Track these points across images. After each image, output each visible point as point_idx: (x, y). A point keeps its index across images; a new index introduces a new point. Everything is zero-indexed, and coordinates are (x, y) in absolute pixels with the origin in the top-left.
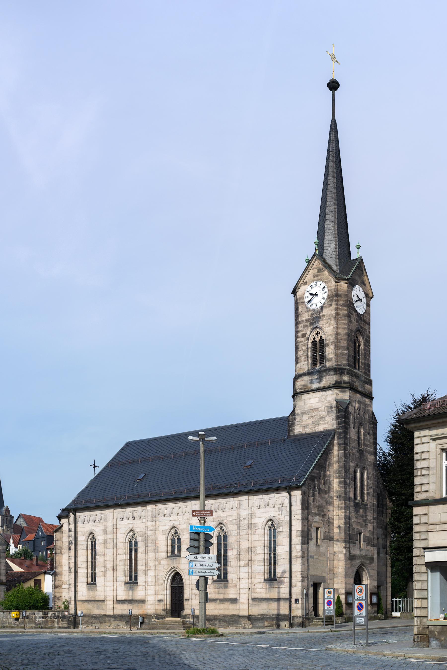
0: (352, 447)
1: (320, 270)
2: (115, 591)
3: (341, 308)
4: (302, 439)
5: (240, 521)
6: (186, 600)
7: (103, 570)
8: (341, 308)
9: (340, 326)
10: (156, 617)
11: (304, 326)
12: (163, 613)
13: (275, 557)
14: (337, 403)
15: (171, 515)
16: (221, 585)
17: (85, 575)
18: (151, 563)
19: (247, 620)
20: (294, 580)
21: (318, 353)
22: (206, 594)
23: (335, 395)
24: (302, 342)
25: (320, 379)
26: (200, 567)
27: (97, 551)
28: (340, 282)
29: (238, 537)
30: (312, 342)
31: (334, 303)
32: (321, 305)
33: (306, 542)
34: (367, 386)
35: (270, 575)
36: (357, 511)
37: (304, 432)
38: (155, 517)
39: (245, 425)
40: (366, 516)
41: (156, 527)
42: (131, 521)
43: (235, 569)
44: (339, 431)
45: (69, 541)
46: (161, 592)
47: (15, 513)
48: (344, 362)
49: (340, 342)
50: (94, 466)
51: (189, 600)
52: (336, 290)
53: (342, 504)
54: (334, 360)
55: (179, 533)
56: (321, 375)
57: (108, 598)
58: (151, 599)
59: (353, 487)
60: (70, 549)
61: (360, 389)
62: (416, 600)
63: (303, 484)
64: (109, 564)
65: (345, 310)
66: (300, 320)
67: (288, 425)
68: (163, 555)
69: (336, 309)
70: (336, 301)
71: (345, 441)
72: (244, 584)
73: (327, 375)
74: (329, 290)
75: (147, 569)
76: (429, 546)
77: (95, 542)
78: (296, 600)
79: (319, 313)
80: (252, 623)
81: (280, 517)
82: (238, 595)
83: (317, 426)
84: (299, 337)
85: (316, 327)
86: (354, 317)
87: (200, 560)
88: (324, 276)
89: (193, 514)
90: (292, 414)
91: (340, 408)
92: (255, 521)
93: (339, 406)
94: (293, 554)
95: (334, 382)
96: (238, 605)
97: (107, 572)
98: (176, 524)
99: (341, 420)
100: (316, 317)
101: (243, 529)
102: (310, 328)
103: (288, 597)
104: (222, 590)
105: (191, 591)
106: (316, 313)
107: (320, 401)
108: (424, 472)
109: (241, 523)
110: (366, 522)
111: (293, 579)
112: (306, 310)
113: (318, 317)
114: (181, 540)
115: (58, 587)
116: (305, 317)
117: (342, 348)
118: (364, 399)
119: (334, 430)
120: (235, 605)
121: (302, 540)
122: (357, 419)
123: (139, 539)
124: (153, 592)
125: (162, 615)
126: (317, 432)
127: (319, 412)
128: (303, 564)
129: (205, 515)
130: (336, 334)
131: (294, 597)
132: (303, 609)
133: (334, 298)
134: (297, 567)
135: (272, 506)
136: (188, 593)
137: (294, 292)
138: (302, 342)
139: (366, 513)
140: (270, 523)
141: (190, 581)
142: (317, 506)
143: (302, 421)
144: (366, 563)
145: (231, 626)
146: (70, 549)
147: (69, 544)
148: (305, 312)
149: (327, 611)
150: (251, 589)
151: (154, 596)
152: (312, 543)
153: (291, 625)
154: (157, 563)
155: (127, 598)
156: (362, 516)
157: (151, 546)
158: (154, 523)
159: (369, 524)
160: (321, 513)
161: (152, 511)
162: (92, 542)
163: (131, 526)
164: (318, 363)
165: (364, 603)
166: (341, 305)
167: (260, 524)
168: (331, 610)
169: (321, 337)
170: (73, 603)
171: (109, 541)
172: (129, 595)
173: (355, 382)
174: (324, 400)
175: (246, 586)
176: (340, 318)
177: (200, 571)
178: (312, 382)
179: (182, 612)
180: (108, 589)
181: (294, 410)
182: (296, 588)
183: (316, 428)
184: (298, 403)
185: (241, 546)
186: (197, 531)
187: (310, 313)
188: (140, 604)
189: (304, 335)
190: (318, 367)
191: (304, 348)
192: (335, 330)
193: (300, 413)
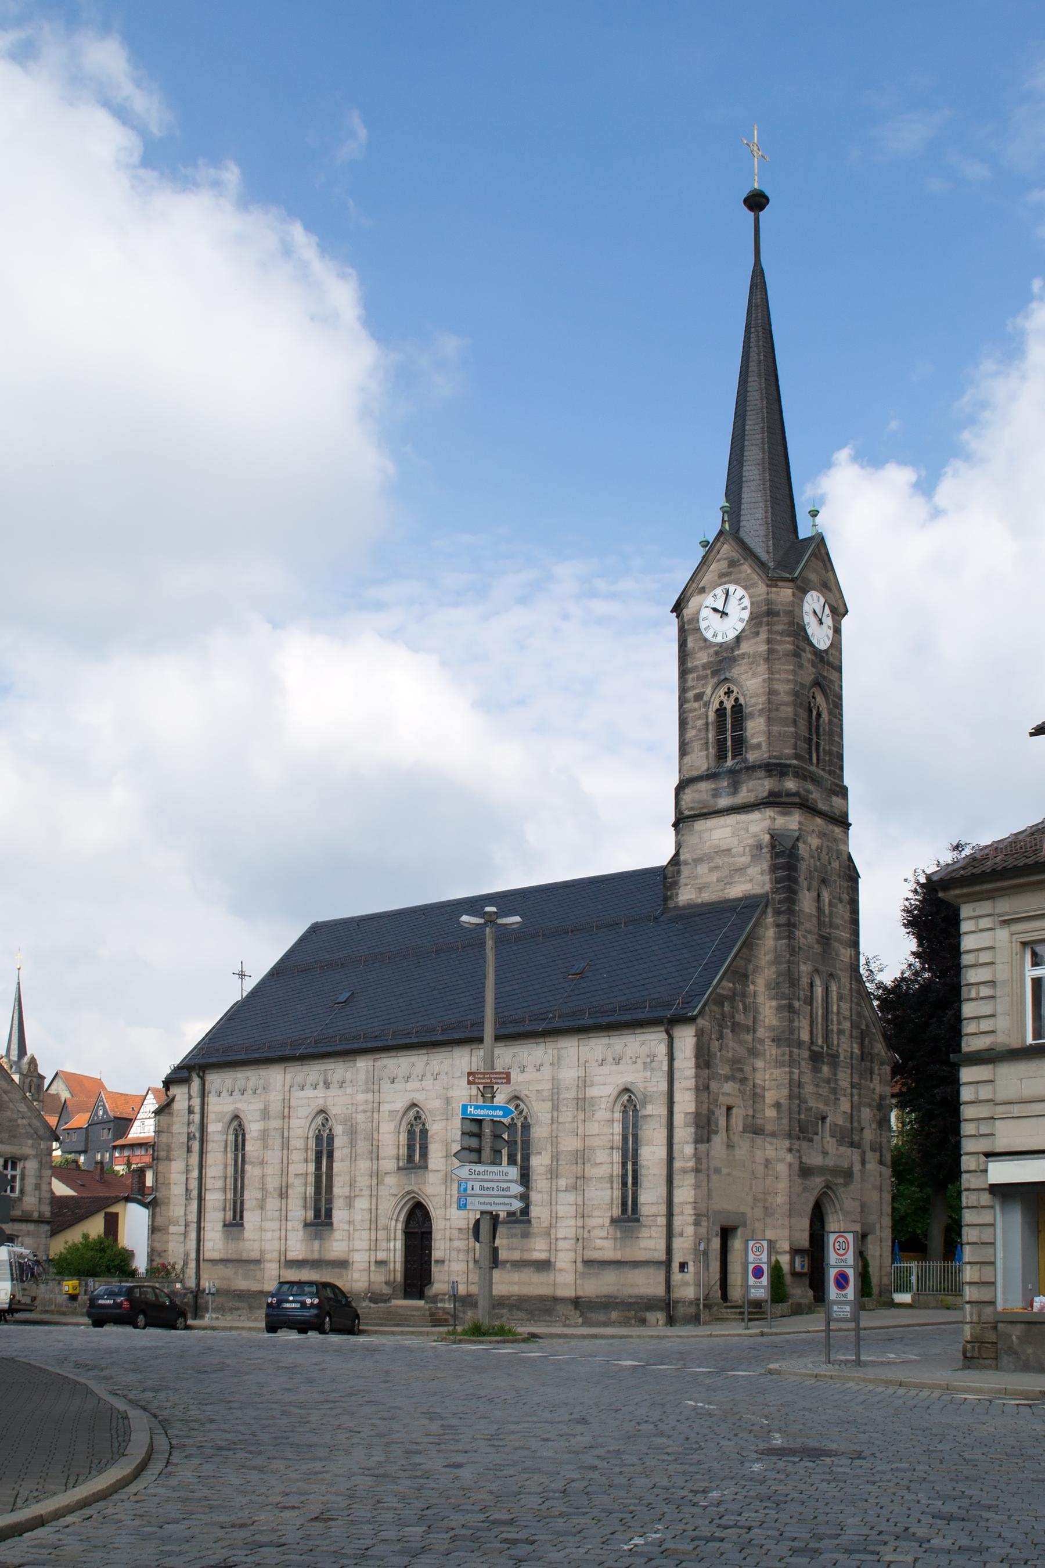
0: (806, 931)
1: (732, 563)
2: (283, 1242)
3: (778, 638)
5: (558, 1093)
6: (437, 1261)
7: (259, 1196)
8: (778, 638)
9: (777, 676)
11: (699, 678)
12: (387, 1290)
13: (635, 1172)
14: (772, 837)
15: (407, 1079)
17: (220, 1205)
18: (363, 1182)
19: (571, 1307)
20: (677, 1221)
21: (729, 733)
24: (695, 710)
26: (482, 1192)
27: (247, 1156)
28: (776, 586)
29: (555, 1126)
30: (717, 710)
31: (764, 629)
32: (737, 633)
33: (706, 1138)
34: (836, 801)
35: (624, 1210)
36: (816, 1070)
37: (699, 901)
38: (373, 1085)
40: (836, 1080)
42: (320, 1092)
43: (546, 1197)
45: (188, 1134)
46: (383, 1245)
47: (46, 1071)
48: (787, 751)
49: (777, 710)
50: (242, 975)
51: (443, 1262)
52: (768, 602)
53: (784, 1055)
55: (423, 1117)
57: (267, 1256)
58: (360, 1259)
59: (808, 1017)
60: (189, 1150)
61: (822, 806)
62: (968, 1267)
63: (701, 1012)
64: (273, 1183)
65: (788, 643)
66: (690, 665)
67: (664, 886)
68: (389, 1164)
69: (769, 641)
70: (768, 625)
71: (789, 919)
72: (566, 1229)
73: (750, 778)
74: (752, 604)
76: (998, 1150)
77: (244, 1135)
78: (683, 1266)
79: (733, 650)
80: (582, 1315)
81: (647, 1084)
82: (553, 1252)
84: (689, 702)
85: (726, 679)
86: (808, 655)
87: (481, 1177)
88: (743, 575)
91: (778, 849)
92: (592, 1092)
94: (677, 1164)
95: (766, 794)
96: (552, 1275)
97: (268, 1200)
98: (419, 1097)
99: (782, 873)
100: (725, 658)
101: (565, 1109)
102: (712, 681)
103: (663, 1257)
104: (516, 1241)
105: (448, 1242)
106: (726, 649)
107: (734, 834)
108: (985, 991)
109: (562, 1096)
111: (675, 1218)
113: (728, 658)
114: (429, 1134)
115: (159, 1230)
116: (702, 658)
117: (783, 721)
118: (831, 827)
119: (766, 895)
120: (545, 1274)
121: (696, 1133)
122: (816, 870)
123: (338, 1130)
124: (365, 1245)
126: (730, 901)
127: (733, 857)
128: (697, 1186)
130: (769, 694)
132: (697, 1285)
133: (765, 619)
134: (685, 1194)
135: (629, 1061)
136: (442, 1247)
137: (678, 608)
138: (695, 710)
139: (835, 1074)
140: (626, 1097)
141: (448, 1222)
142: (728, 1061)
143: (695, 878)
144: (836, 1184)
146: (189, 1150)
147: (189, 1139)
148: (701, 649)
149: (753, 1291)
150: (581, 1241)
151: (367, 1254)
152: (718, 1141)
153: (671, 1321)
154: (374, 1182)
155: (309, 1257)
156: (828, 1081)
157: (363, 1146)
158: (370, 1096)
159: (843, 1098)
160: (738, 1075)
161: (367, 1072)
162: (236, 1136)
163: (320, 1103)
164: (730, 754)
165: (850, 1273)
166: (781, 634)
169: (737, 699)
170: (193, 1265)
171: (272, 1133)
172: (312, 1251)
173: (812, 793)
174: (742, 832)
175: (571, 1233)
177: (482, 1200)
178: (716, 794)
180: (268, 1235)
184: (684, 838)
185: (561, 1147)
187: (712, 651)
188: (337, 1270)
189: (698, 697)
190: (729, 763)
191: (700, 723)
193: (690, 861)
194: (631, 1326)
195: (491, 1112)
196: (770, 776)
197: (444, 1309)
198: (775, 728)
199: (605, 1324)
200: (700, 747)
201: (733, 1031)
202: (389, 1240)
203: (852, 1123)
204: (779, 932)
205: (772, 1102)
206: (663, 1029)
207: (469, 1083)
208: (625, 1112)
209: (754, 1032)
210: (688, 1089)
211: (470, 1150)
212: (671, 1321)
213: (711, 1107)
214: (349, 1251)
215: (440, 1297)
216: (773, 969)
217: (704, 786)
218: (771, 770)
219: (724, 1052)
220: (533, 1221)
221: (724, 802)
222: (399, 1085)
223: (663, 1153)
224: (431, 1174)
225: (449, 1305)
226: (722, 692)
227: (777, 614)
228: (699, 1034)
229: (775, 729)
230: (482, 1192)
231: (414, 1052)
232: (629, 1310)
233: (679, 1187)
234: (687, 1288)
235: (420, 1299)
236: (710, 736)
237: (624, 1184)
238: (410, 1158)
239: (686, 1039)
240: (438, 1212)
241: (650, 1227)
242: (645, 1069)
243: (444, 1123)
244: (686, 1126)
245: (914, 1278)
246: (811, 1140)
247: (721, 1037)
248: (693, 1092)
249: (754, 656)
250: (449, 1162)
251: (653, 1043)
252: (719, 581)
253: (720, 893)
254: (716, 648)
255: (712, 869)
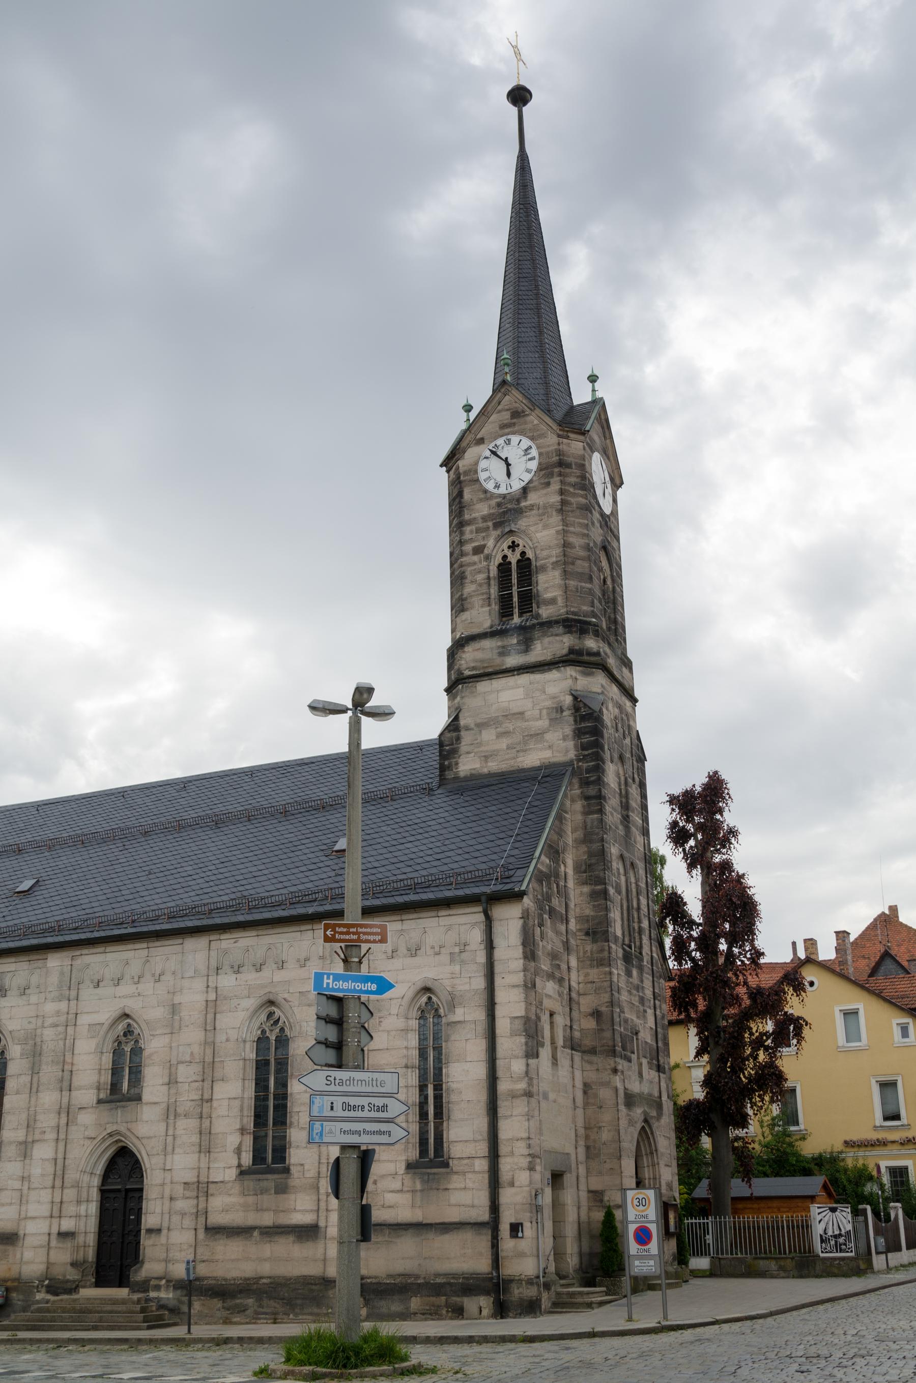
3: (571, 490)
4: (483, 787)
6: (150, 1231)
8: (571, 490)
9: (572, 529)
10: (48, 1286)
11: (478, 531)
12: (72, 1275)
13: (438, 1098)
14: (575, 698)
15: (118, 982)
16: (265, 1184)
18: (47, 1121)
20: (506, 1165)
21: (515, 588)
22: (365, 1211)
23: (570, 681)
24: (475, 563)
25: (527, 644)
26: (347, 1114)
28: (567, 438)
30: (500, 565)
32: (523, 484)
34: (625, 671)
35: (423, 1151)
36: (629, 974)
37: (485, 771)
38: (70, 990)
39: (306, 764)
41: (71, 1016)
44: (585, 765)
46: (70, 1209)
48: (585, 608)
49: (573, 564)
51: (159, 1231)
52: (559, 453)
53: (602, 950)
54: (560, 601)
55: (136, 1032)
56: (528, 635)
58: (36, 1230)
65: (582, 496)
66: (467, 517)
68: (86, 1096)
69: (561, 492)
70: (560, 475)
73: (545, 635)
74: (540, 454)
75: (30, 1139)
78: (516, 1229)
79: (518, 501)
81: (457, 981)
82: (322, 1214)
83: (521, 754)
84: (466, 555)
85: (511, 532)
86: (596, 515)
87: (344, 1088)
88: (529, 426)
89: (325, 935)
90: (452, 728)
91: (583, 711)
93: (581, 705)
94: (503, 1086)
95: (565, 651)
98: (133, 1005)
100: (510, 510)
102: (495, 534)
103: (485, 1216)
104: (268, 1200)
106: (510, 501)
110: (643, 1005)
111: (502, 1161)
112: (482, 496)
113: (514, 509)
114: (146, 1053)
116: (482, 509)
119: (570, 763)
124: (45, 1210)
125: (68, 1281)
126: (523, 770)
129: (363, 937)
130: (564, 546)
131: (507, 1218)
133: (556, 470)
135: (430, 952)
136: (158, 1210)
137: (449, 462)
138: (475, 563)
139: (642, 981)
140: (424, 999)
141: (168, 1175)
143: (480, 744)
145: (296, 1315)
148: (481, 500)
149: (637, 1263)
151: (47, 1222)
152: (545, 1053)
154: (63, 1120)
156: (637, 988)
158: (63, 1006)
161: (62, 973)
164: (516, 610)
165: (653, 1228)
166: (574, 486)
167: (395, 1001)
168: (651, 1257)
169: (523, 553)
174: (538, 694)
176: (572, 511)
177: (347, 1126)
178: (503, 652)
179: (136, 1271)
181: (456, 718)
182: (513, 1190)
183: (519, 759)
184: (466, 700)
186: (339, 990)
187: (493, 502)
189: (478, 550)
190: (516, 620)
191: (481, 577)
192: (560, 537)
193: (472, 726)
194: (441, 1318)
195: (359, 986)
196: (570, 632)
197: (158, 1299)
198: (572, 582)
199: (404, 1316)
200: (481, 602)
201: (550, 915)
202: (79, 1202)
203: (657, 1043)
204: (589, 805)
205: (590, 1010)
206: (480, 909)
207: (327, 939)
208: (422, 1017)
209: (567, 923)
210: (514, 986)
211: (326, 1044)
212: (501, 1310)
213: (538, 1011)
214: (20, 1220)
215: (153, 1283)
216: (584, 848)
217: (487, 643)
218: (570, 626)
219: (545, 943)
220: (293, 1170)
221: (512, 661)
222: (106, 990)
223: (480, 1071)
224: (146, 1109)
225: (167, 1295)
226: (505, 546)
227: (569, 466)
228: (525, 916)
229: (572, 583)
230: (347, 1114)
231: (130, 946)
232: (438, 1295)
233: (506, 1117)
234: (525, 1259)
235: (120, 1285)
236: (492, 591)
237: (423, 1115)
238: (115, 1087)
239: (509, 920)
240: (154, 1160)
241: (464, 1173)
242: (452, 961)
243: (167, 1039)
244: (513, 1034)
245: (709, 1238)
246: (630, 1061)
247: (541, 925)
248: (521, 990)
249: (545, 507)
250: (173, 1091)
251: (462, 928)
252: (501, 432)
253: (512, 762)
254: (499, 500)
255: (500, 735)
